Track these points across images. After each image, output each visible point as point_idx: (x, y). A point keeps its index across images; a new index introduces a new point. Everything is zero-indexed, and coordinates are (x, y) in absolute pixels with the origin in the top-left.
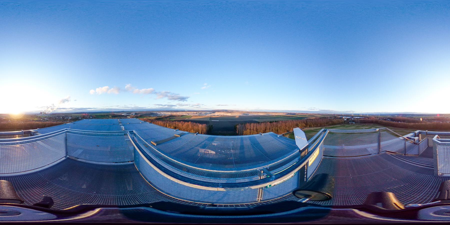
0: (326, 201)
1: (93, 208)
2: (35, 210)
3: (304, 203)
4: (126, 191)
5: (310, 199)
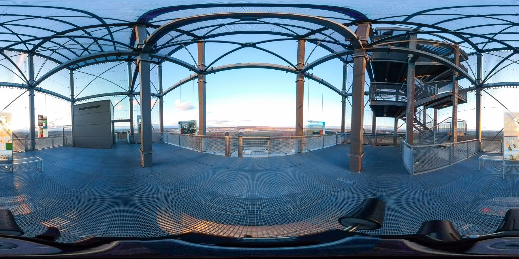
1: (108, 240)
2: (36, 243)
3: (351, 232)
4: (135, 218)
5: (357, 228)
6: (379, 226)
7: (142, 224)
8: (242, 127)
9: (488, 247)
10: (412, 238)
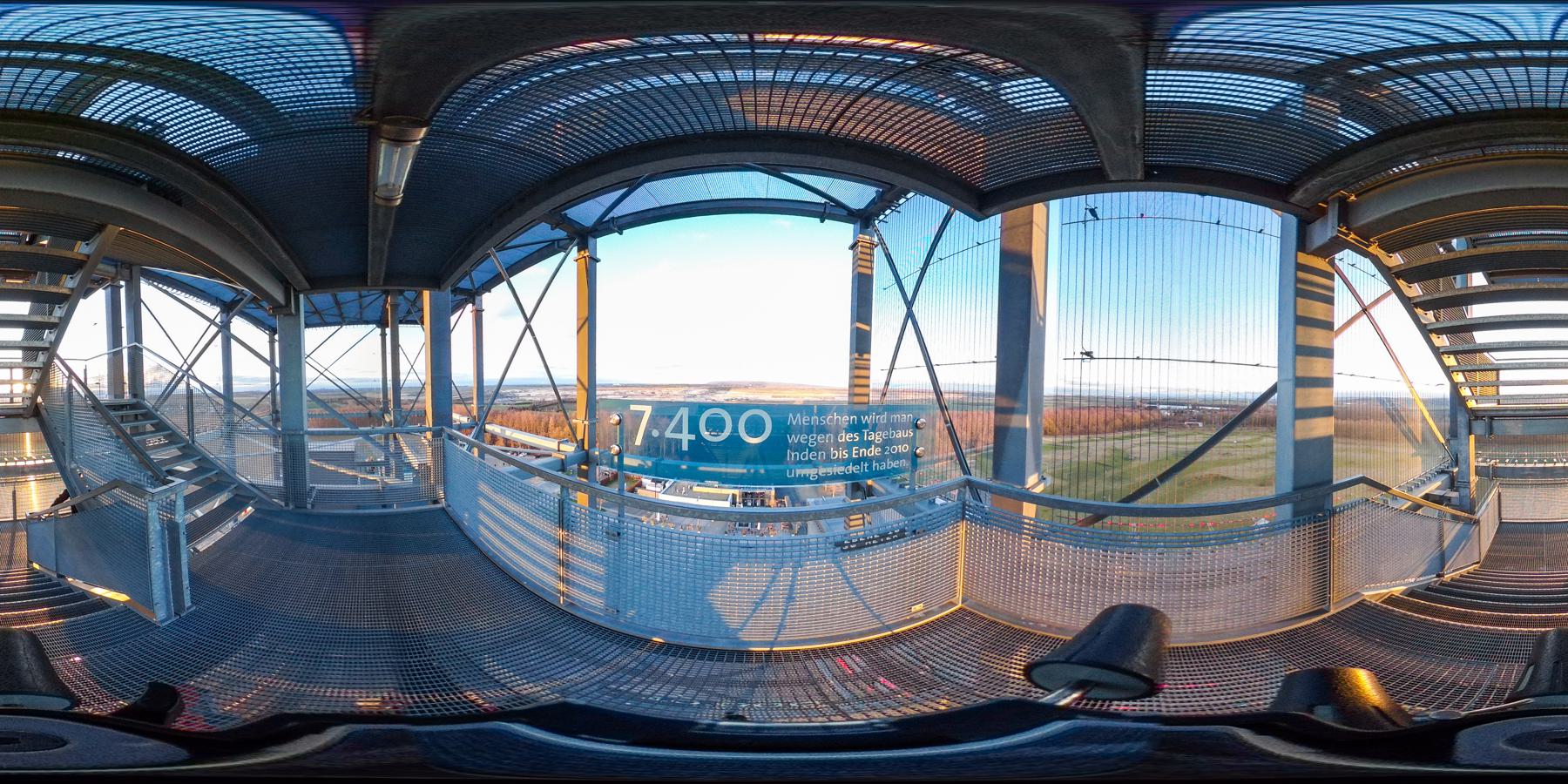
1: (317, 723)
2: (131, 736)
6: (1152, 689)
8: (722, 383)
10: (1257, 722)
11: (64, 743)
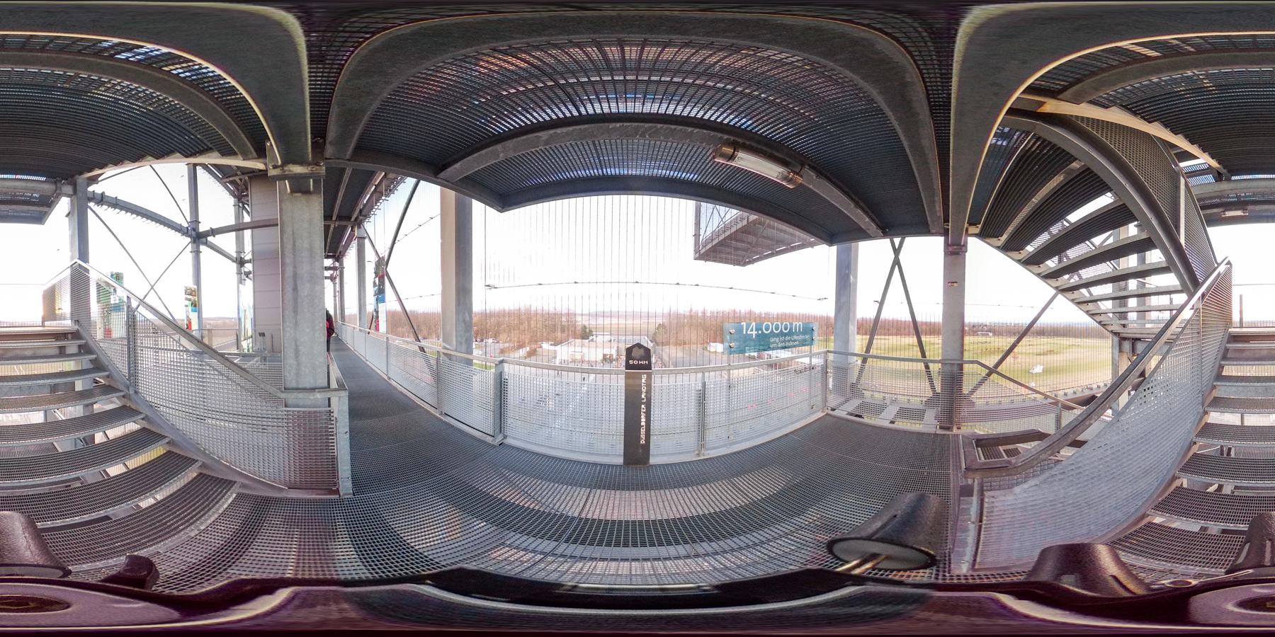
0: (925, 571)
1: (268, 587)
2: (117, 598)
5: (874, 566)
7: (366, 551)
9: (1230, 607)
11: (68, 606)
